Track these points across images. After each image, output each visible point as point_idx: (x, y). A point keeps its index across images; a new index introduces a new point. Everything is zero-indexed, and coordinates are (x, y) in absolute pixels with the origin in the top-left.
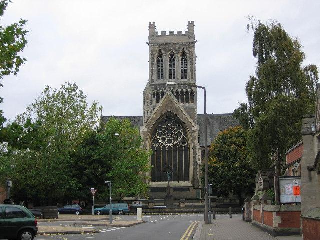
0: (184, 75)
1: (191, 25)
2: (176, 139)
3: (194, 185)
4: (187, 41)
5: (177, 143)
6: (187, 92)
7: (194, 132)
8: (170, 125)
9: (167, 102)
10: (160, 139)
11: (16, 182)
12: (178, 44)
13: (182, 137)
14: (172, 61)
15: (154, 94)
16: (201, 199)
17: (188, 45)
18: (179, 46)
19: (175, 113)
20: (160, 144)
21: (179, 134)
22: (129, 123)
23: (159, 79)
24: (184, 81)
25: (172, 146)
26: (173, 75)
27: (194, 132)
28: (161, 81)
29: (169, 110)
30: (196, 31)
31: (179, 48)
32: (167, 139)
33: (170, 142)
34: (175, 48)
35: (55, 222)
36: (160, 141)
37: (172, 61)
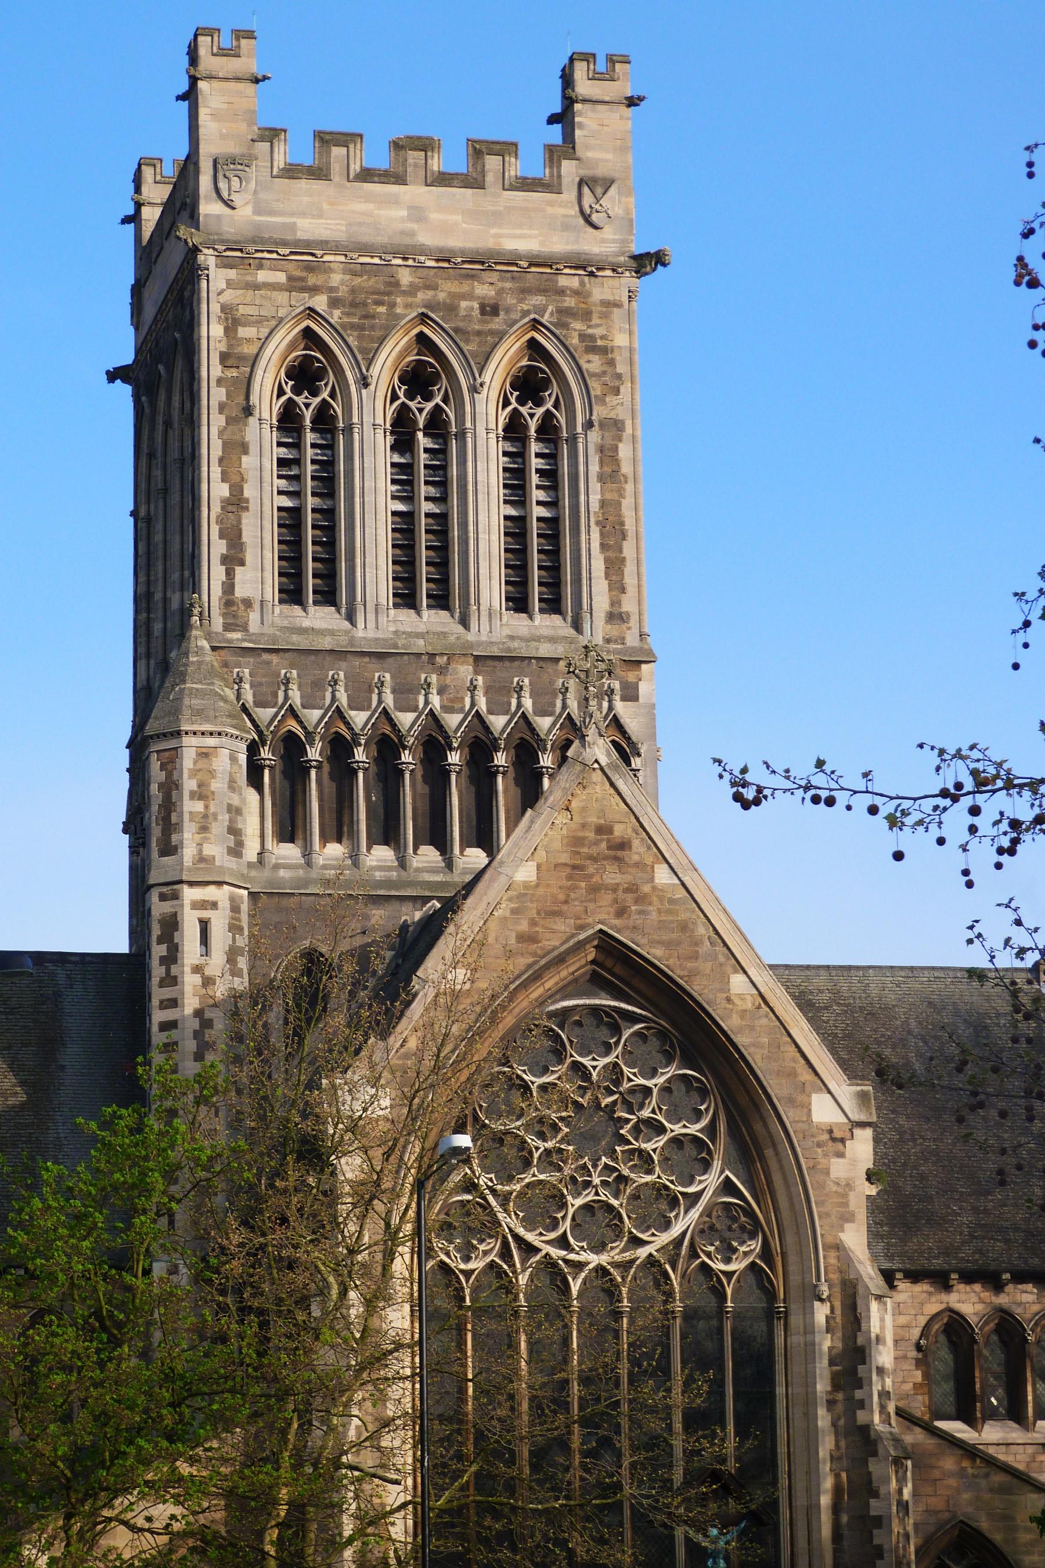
0: (541, 573)
1: (112, 376)
2: (661, 1204)
4: (558, 245)
5: (665, 1238)
6: (435, 744)
7: (837, 1140)
8: (596, 1064)
9: (576, 842)
10: (504, 1199)
12: (483, 261)
13: (710, 1181)
14: (424, 435)
15: (253, 749)
17: (568, 281)
18: (484, 290)
19: (655, 954)
20: (505, 1253)
21: (694, 1155)
22: (30, 967)
25: (625, 1266)
26: (428, 571)
27: (837, 1140)
29: (600, 917)
31: (490, 309)
33: (600, 1225)
34: (451, 309)
36: (510, 1221)
37: (424, 435)
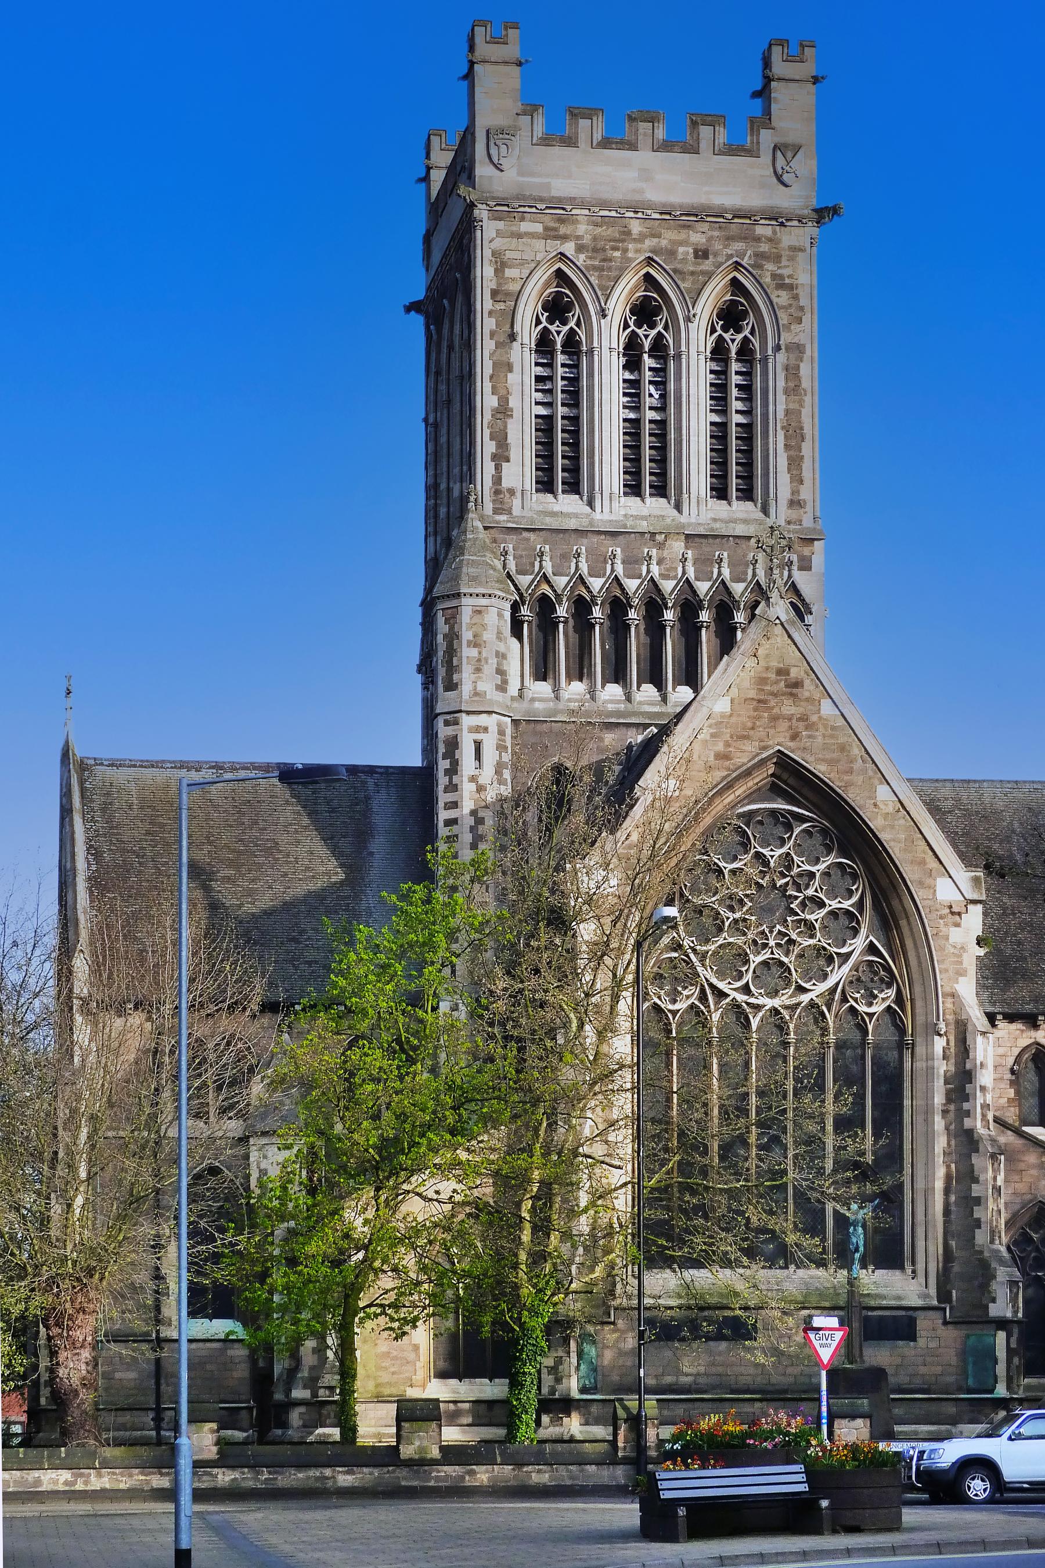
3: (944, 1295)
4: (755, 200)
8: (774, 854)
9: (762, 681)
11: (285, 1258)
13: (859, 943)
14: (649, 354)
16: (1001, 1391)
18: (697, 238)
19: (820, 769)
20: (703, 997)
21: (849, 922)
23: (546, 485)
24: (738, 515)
26: (651, 467)
28: (567, 506)
29: (780, 741)
30: (461, 75)
31: (702, 254)
32: (756, 959)
34: (671, 253)
35: (1015, 1518)
36: (707, 974)
37: (649, 354)
